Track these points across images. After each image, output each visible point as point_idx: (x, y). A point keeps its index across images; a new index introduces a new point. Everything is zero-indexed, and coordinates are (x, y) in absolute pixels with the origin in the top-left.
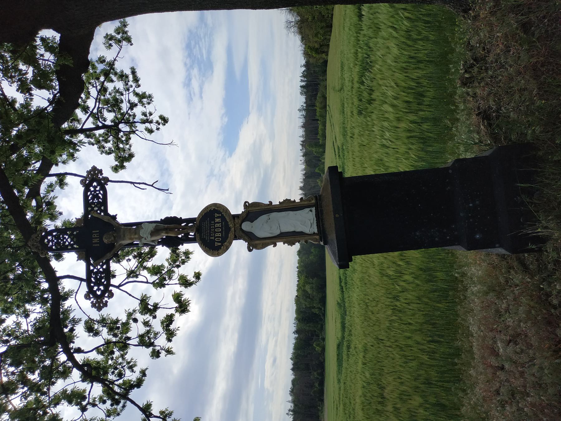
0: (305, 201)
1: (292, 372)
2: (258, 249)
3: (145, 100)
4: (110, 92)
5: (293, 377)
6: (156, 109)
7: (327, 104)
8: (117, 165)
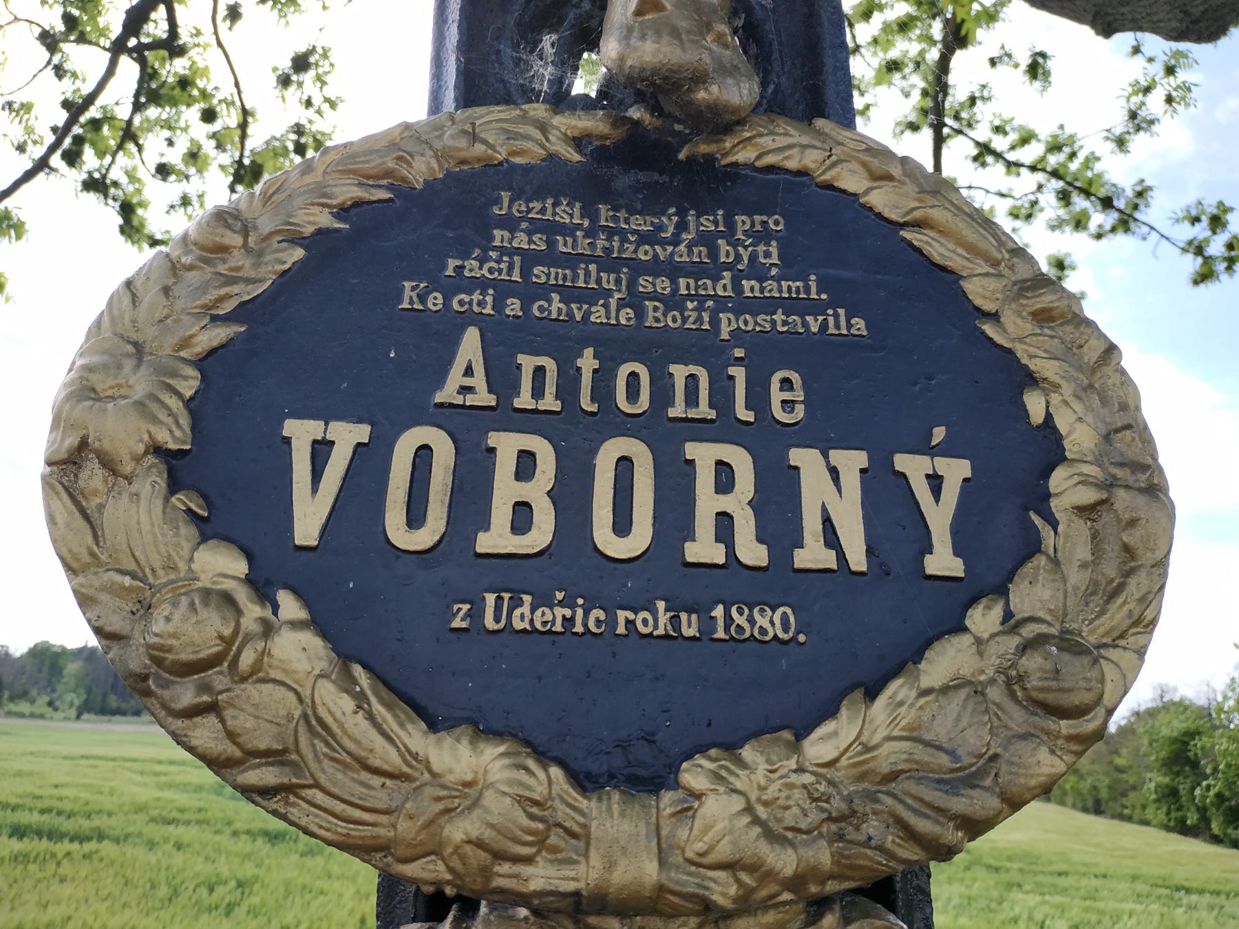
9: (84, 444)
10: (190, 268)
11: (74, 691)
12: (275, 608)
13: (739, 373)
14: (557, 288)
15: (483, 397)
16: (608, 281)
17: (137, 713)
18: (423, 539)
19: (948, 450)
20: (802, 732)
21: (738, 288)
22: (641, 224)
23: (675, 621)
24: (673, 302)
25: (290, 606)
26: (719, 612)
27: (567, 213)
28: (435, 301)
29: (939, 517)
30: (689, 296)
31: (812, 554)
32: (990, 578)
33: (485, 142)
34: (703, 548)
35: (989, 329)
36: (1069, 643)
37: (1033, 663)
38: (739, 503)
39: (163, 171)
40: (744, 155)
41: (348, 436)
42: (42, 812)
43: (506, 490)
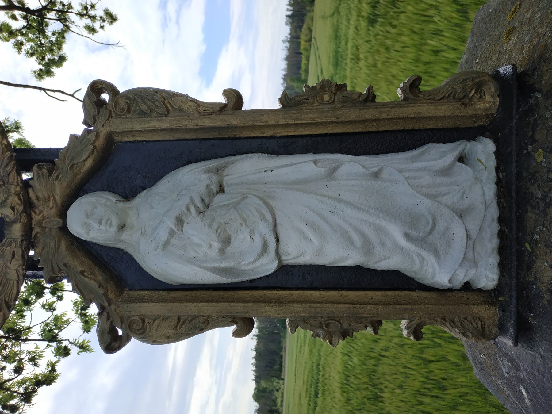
0: (435, 97)
2: (155, 342)
7: (313, 36)
11: (273, 382)
17: (281, 357)
42: (311, 387)
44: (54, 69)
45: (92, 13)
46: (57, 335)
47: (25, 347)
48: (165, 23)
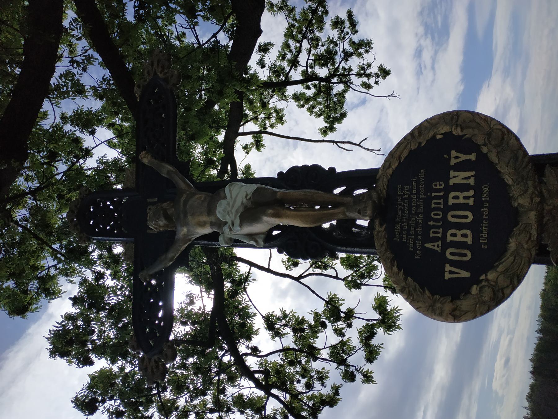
1: (531, 375)
3: (362, 51)
4: (322, 43)
5: (532, 381)
6: (375, 58)
8: (326, 127)
9: (450, 314)
10: (413, 298)
12: (483, 279)
13: (433, 194)
14: (415, 229)
15: (440, 243)
16: (413, 219)
18: (469, 254)
19: (449, 155)
20: (507, 185)
21: (414, 194)
22: (400, 213)
23: (486, 207)
24: (417, 207)
25: (483, 277)
26: (483, 199)
27: (398, 227)
28: (419, 252)
29: (463, 157)
30: (416, 203)
31: (472, 181)
32: (476, 148)
33: (383, 243)
34: (471, 202)
35: (423, 145)
36: (489, 135)
37: (493, 143)
38: (461, 195)
39: (309, 386)
40: (384, 192)
41: (448, 268)
43: (459, 239)
44: (336, 126)
45: (368, 72)
46: (346, 359)
47: (316, 365)
48: (419, 72)
